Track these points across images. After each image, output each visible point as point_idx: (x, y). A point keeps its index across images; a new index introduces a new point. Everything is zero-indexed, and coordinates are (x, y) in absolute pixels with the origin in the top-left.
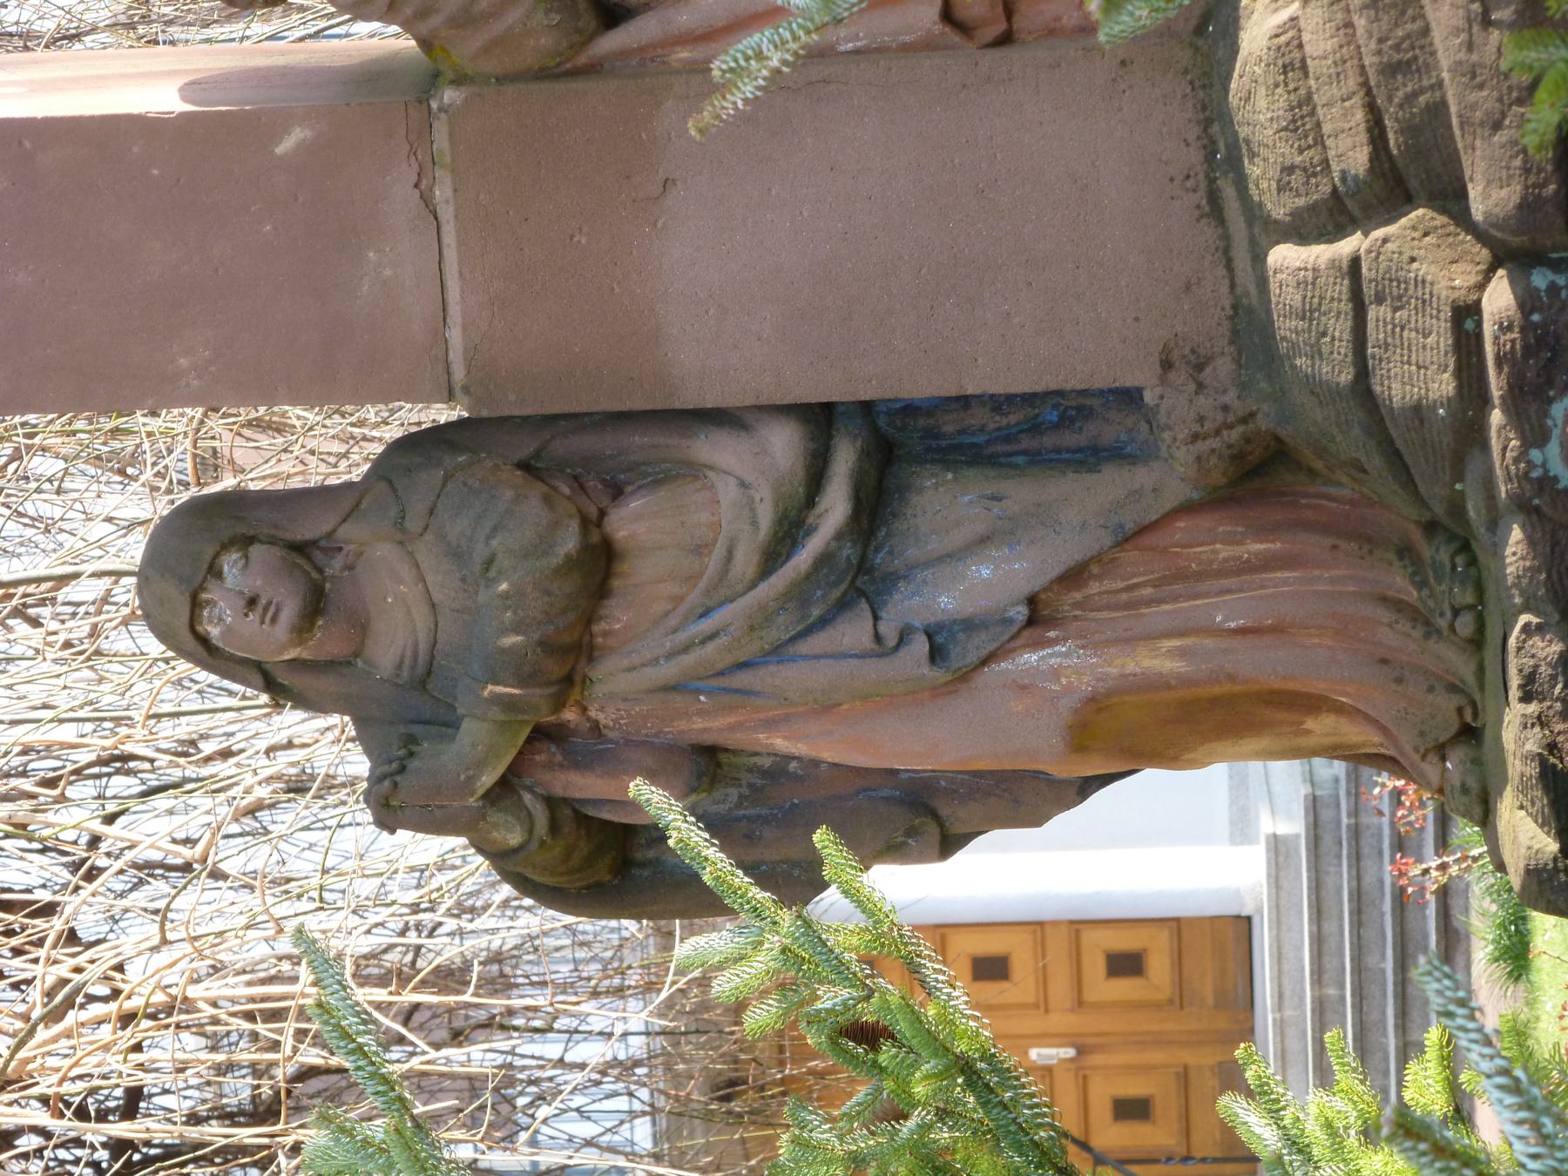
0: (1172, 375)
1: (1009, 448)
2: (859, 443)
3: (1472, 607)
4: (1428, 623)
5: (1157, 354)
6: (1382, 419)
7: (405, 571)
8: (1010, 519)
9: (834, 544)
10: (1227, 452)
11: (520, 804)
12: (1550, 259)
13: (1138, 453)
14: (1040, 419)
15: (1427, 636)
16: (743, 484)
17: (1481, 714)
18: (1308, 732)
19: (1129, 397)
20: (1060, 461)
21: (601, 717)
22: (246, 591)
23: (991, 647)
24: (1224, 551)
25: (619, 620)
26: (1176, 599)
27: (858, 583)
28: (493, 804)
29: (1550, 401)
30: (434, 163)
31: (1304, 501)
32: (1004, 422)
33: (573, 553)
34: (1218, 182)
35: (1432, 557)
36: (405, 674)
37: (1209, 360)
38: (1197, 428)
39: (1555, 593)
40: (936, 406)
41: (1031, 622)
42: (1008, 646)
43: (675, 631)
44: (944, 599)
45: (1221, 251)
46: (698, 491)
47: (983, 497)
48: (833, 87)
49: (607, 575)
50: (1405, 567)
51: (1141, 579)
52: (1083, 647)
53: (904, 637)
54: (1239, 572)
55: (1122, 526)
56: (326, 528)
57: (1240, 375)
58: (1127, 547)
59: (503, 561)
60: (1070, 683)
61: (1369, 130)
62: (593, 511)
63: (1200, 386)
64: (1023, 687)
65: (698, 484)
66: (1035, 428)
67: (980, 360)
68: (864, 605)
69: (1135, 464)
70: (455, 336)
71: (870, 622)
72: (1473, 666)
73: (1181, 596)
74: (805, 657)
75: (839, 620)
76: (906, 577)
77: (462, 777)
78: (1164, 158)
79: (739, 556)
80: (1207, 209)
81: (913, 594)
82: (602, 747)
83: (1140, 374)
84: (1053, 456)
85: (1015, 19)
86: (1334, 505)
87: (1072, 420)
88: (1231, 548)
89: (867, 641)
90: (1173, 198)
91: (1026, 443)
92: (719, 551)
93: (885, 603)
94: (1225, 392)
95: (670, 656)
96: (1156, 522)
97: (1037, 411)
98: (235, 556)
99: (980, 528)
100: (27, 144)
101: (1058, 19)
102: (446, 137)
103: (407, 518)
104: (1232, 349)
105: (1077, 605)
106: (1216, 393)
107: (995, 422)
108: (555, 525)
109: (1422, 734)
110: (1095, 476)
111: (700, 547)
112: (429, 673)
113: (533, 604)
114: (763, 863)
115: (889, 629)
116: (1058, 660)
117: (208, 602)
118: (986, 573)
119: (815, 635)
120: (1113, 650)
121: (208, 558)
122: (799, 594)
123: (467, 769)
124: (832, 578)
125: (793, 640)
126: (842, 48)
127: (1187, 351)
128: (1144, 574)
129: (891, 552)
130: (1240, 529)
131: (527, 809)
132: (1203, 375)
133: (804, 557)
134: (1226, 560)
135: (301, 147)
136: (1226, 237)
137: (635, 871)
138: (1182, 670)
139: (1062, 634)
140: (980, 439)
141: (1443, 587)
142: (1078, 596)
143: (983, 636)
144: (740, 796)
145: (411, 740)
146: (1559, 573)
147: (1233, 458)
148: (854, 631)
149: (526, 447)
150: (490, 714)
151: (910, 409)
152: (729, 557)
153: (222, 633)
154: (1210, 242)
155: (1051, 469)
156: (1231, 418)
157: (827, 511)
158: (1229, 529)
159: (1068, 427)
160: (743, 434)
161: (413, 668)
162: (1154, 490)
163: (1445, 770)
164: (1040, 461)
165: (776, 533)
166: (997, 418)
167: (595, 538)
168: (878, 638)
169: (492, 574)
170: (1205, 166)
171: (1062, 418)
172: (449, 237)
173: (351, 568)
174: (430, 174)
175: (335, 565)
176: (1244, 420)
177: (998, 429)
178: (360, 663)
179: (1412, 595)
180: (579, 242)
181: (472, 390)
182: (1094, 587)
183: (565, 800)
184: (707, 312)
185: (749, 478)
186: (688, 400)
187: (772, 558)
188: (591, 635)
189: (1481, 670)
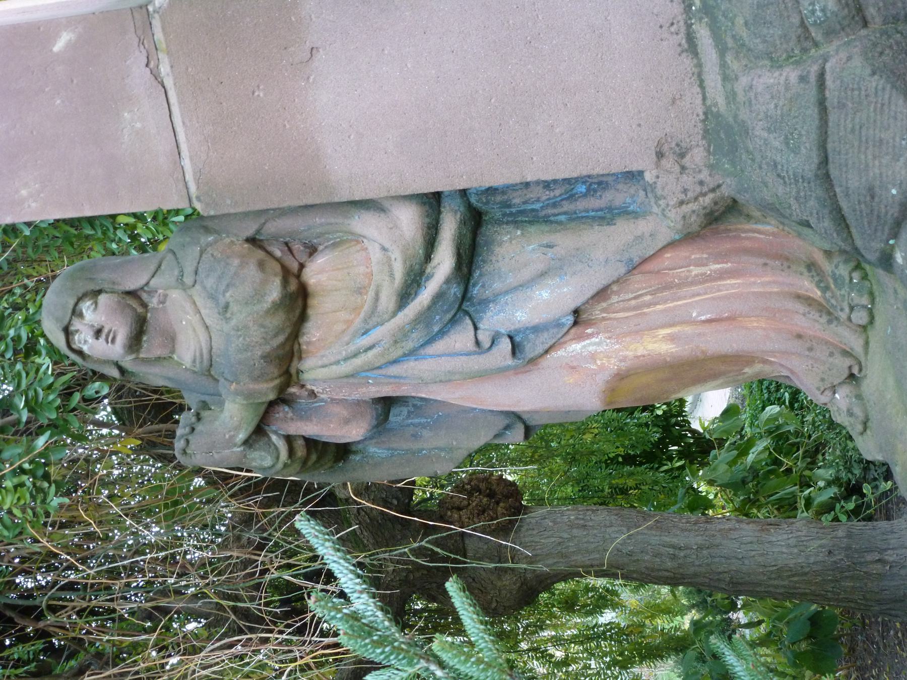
0: (664, 162)
1: (556, 211)
2: (458, 216)
5: (653, 148)
7: (188, 307)
9: (444, 286)
10: (702, 212)
11: (270, 442)
13: (638, 210)
14: (574, 191)
15: (830, 322)
16: (384, 249)
17: (864, 370)
20: (587, 217)
22: (96, 325)
23: (550, 343)
24: (695, 271)
25: (315, 336)
26: (665, 301)
27: (464, 307)
28: (251, 446)
30: (156, 49)
31: (743, 235)
32: (552, 194)
33: (277, 298)
34: (694, 27)
35: (832, 272)
37: (688, 150)
38: (683, 197)
40: (507, 187)
41: (576, 323)
42: (562, 340)
43: (348, 344)
44: (518, 314)
45: (695, 76)
46: (358, 251)
47: (540, 246)
50: (813, 276)
51: (644, 291)
52: (610, 338)
54: (705, 282)
55: (631, 260)
57: (709, 159)
58: (635, 272)
59: (234, 307)
60: (603, 364)
62: (295, 266)
63: (683, 168)
64: (573, 368)
65: (358, 247)
66: (572, 197)
67: (535, 159)
68: (468, 321)
69: (637, 218)
70: (187, 163)
72: (861, 342)
73: (668, 300)
74: (432, 356)
75: (452, 331)
76: (494, 301)
77: (227, 436)
78: (655, 11)
80: (686, 46)
82: (318, 404)
83: (644, 163)
84: (584, 214)
86: (762, 236)
87: (595, 191)
88: (699, 268)
89: (470, 345)
90: (662, 40)
91: (567, 206)
92: (371, 294)
93: (482, 318)
94: (700, 171)
95: (346, 359)
96: (653, 255)
97: (572, 187)
98: (88, 303)
99: (540, 267)
102: (160, 30)
103: (185, 275)
104: (704, 142)
105: (604, 310)
106: (694, 172)
107: (545, 195)
108: (264, 282)
112: (211, 365)
113: (255, 333)
114: (423, 449)
115: (484, 337)
116: (594, 347)
117: (77, 331)
118: (545, 294)
119: (437, 342)
120: (628, 339)
121: (71, 306)
122: (424, 318)
123: (230, 431)
124: (445, 307)
127: (673, 145)
128: (645, 288)
129: (483, 286)
130: (705, 256)
131: (275, 445)
134: (696, 276)
135: (69, 46)
136: (699, 65)
137: (352, 457)
138: (673, 350)
139: (595, 330)
140: (537, 206)
141: (843, 292)
142: (604, 305)
144: (409, 412)
147: (706, 215)
151: (491, 191)
152: (377, 298)
153: (89, 348)
154: (689, 69)
155: (584, 223)
156: (705, 189)
157: (439, 264)
158: (698, 256)
159: (593, 195)
160: (382, 215)
161: (202, 362)
162: (651, 235)
163: (834, 398)
164: (578, 219)
165: (406, 281)
166: (547, 193)
168: (477, 343)
170: (684, 16)
172: (173, 99)
173: (163, 302)
174: (155, 57)
176: (713, 190)
179: (817, 294)
180: (259, 96)
181: (202, 198)
182: (615, 299)
184: (349, 137)
186: (344, 196)
187: (405, 296)
188: (299, 345)
189: (867, 343)
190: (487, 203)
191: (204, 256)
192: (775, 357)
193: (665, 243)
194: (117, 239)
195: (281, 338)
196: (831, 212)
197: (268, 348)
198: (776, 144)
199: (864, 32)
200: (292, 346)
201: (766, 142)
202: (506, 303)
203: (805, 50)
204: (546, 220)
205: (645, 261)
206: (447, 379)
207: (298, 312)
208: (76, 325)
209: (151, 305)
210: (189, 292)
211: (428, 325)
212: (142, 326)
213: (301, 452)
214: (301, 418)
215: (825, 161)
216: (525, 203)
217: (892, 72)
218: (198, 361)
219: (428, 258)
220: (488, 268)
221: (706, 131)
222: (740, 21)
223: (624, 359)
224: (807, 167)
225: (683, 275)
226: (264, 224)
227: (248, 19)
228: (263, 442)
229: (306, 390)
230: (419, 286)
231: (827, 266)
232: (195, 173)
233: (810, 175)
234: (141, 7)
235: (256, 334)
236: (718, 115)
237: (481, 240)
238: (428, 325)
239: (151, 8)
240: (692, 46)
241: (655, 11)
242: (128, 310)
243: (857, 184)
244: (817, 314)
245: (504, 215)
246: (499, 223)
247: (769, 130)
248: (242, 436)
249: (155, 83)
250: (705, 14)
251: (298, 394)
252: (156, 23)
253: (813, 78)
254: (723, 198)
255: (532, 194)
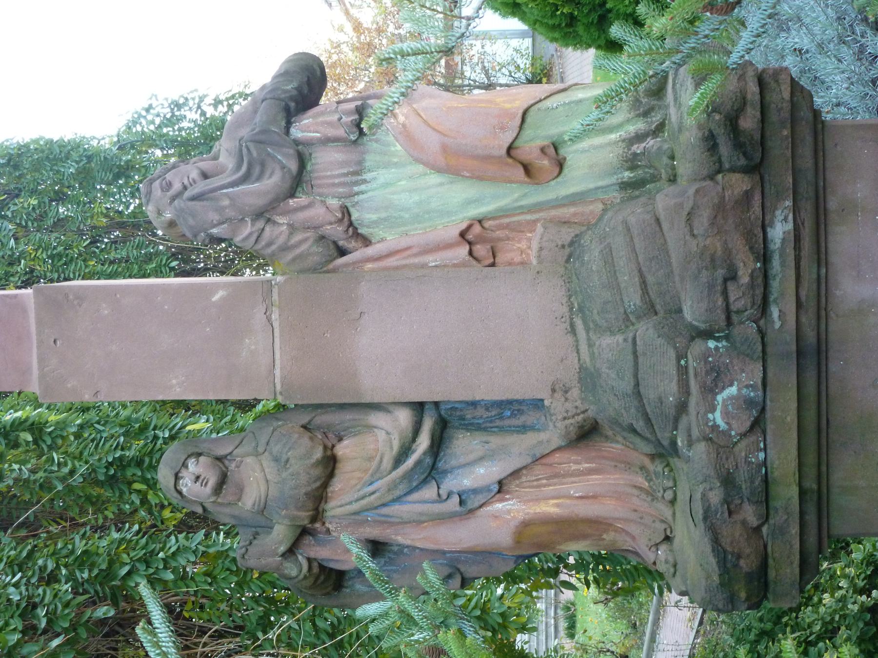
0: (556, 395)
3: (672, 488)
4: (652, 495)
6: (644, 405)
7: (257, 468)
8: (492, 450)
12: (715, 336)
15: (653, 500)
18: (604, 539)
19: (538, 404)
21: (330, 526)
24: (574, 467)
26: (555, 485)
28: (286, 559)
29: (717, 394)
32: (490, 414)
36: (256, 507)
37: (570, 389)
38: (565, 415)
39: (718, 474)
41: (499, 492)
42: (490, 501)
44: (465, 481)
48: (426, 278)
49: (334, 468)
53: (449, 495)
54: (579, 475)
55: (535, 455)
56: (229, 451)
58: (536, 463)
59: (292, 461)
61: (641, 285)
62: (330, 445)
63: (566, 399)
64: (496, 517)
65: (371, 435)
68: (434, 483)
70: (278, 372)
71: (436, 489)
72: (670, 513)
75: (424, 488)
76: (450, 472)
79: (385, 461)
81: (454, 479)
83: (544, 394)
85: (496, 259)
87: (516, 415)
92: (378, 458)
93: (443, 482)
94: (576, 401)
95: (357, 500)
98: (193, 460)
100: (118, 296)
101: (513, 259)
105: (517, 486)
108: (313, 448)
109: (650, 540)
110: (525, 436)
111: (370, 458)
112: (265, 508)
115: (443, 492)
118: (482, 471)
120: (531, 503)
122: (408, 476)
125: (405, 495)
126: (430, 265)
129: (445, 462)
132: (568, 395)
133: (410, 462)
134: (574, 470)
135: (223, 299)
136: (577, 341)
137: (344, 590)
140: (480, 421)
142: (517, 482)
143: (481, 496)
144: (385, 562)
145: (257, 533)
146: (720, 466)
148: (429, 492)
149: (305, 419)
150: (284, 522)
153: (187, 490)
156: (579, 411)
160: (389, 414)
161: (259, 505)
162: (547, 441)
163: (657, 554)
167: (329, 453)
168: (439, 495)
169: (288, 466)
171: (512, 414)
173: (238, 467)
175: (232, 466)
176: (583, 412)
177: (487, 417)
178: (240, 504)
179: (646, 485)
182: (524, 479)
183: (315, 559)
185: (390, 430)
187: (398, 461)
189: (674, 514)
190: (451, 415)
191: (275, 433)
192: (621, 523)
193: (555, 447)
194: (130, 502)
195: (318, 484)
196: (643, 415)
197: (309, 489)
198: (613, 376)
199: (655, 317)
200: (322, 494)
201: (608, 375)
202: (458, 474)
203: (627, 327)
204: (485, 429)
205: (543, 457)
206: (418, 522)
207: (330, 469)
208: (184, 473)
209: (230, 468)
210: (259, 458)
211: (410, 481)
212: (224, 479)
213: (316, 570)
214: (319, 545)
215: (637, 385)
216: (474, 418)
217: (668, 336)
218: (256, 506)
219: (414, 440)
220: (449, 451)
221: (580, 379)
222: (595, 311)
223: (528, 514)
224: (628, 388)
225: (566, 469)
226: (314, 417)
227: (328, 293)
228: (293, 558)
229: (325, 527)
230: (407, 456)
231: (651, 467)
232: (281, 377)
233: (630, 392)
234: (268, 281)
235: (304, 478)
236: (586, 369)
237: (445, 435)
238: (410, 481)
239: (273, 283)
240: (573, 330)
241: (553, 309)
242: (217, 467)
243: (653, 396)
244: (645, 496)
245: (460, 425)
246: (458, 428)
247: (609, 368)
248: (282, 549)
249: (268, 324)
250: (580, 312)
251: (319, 530)
252: (275, 291)
253: (630, 340)
254: (589, 418)
255: (480, 412)
